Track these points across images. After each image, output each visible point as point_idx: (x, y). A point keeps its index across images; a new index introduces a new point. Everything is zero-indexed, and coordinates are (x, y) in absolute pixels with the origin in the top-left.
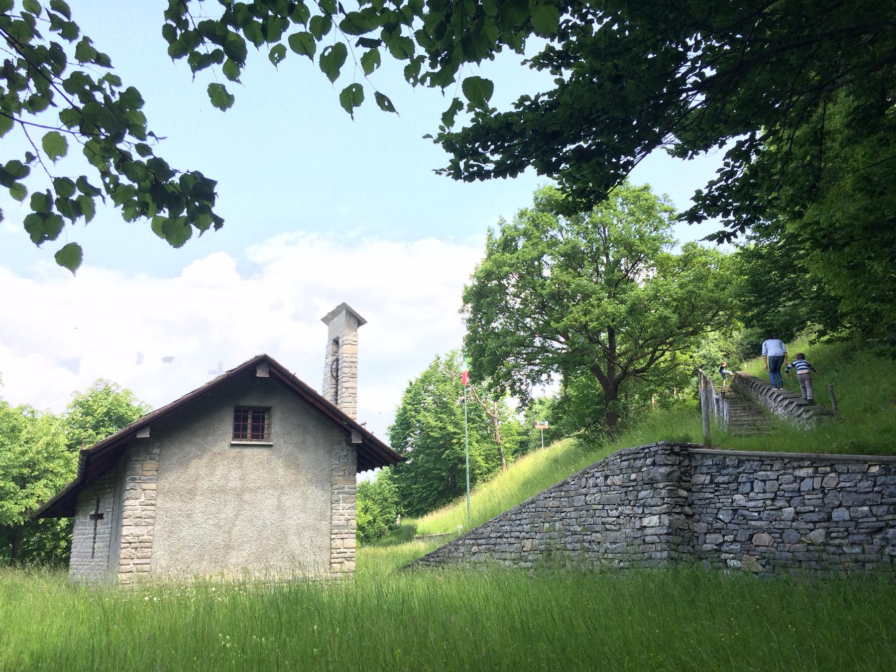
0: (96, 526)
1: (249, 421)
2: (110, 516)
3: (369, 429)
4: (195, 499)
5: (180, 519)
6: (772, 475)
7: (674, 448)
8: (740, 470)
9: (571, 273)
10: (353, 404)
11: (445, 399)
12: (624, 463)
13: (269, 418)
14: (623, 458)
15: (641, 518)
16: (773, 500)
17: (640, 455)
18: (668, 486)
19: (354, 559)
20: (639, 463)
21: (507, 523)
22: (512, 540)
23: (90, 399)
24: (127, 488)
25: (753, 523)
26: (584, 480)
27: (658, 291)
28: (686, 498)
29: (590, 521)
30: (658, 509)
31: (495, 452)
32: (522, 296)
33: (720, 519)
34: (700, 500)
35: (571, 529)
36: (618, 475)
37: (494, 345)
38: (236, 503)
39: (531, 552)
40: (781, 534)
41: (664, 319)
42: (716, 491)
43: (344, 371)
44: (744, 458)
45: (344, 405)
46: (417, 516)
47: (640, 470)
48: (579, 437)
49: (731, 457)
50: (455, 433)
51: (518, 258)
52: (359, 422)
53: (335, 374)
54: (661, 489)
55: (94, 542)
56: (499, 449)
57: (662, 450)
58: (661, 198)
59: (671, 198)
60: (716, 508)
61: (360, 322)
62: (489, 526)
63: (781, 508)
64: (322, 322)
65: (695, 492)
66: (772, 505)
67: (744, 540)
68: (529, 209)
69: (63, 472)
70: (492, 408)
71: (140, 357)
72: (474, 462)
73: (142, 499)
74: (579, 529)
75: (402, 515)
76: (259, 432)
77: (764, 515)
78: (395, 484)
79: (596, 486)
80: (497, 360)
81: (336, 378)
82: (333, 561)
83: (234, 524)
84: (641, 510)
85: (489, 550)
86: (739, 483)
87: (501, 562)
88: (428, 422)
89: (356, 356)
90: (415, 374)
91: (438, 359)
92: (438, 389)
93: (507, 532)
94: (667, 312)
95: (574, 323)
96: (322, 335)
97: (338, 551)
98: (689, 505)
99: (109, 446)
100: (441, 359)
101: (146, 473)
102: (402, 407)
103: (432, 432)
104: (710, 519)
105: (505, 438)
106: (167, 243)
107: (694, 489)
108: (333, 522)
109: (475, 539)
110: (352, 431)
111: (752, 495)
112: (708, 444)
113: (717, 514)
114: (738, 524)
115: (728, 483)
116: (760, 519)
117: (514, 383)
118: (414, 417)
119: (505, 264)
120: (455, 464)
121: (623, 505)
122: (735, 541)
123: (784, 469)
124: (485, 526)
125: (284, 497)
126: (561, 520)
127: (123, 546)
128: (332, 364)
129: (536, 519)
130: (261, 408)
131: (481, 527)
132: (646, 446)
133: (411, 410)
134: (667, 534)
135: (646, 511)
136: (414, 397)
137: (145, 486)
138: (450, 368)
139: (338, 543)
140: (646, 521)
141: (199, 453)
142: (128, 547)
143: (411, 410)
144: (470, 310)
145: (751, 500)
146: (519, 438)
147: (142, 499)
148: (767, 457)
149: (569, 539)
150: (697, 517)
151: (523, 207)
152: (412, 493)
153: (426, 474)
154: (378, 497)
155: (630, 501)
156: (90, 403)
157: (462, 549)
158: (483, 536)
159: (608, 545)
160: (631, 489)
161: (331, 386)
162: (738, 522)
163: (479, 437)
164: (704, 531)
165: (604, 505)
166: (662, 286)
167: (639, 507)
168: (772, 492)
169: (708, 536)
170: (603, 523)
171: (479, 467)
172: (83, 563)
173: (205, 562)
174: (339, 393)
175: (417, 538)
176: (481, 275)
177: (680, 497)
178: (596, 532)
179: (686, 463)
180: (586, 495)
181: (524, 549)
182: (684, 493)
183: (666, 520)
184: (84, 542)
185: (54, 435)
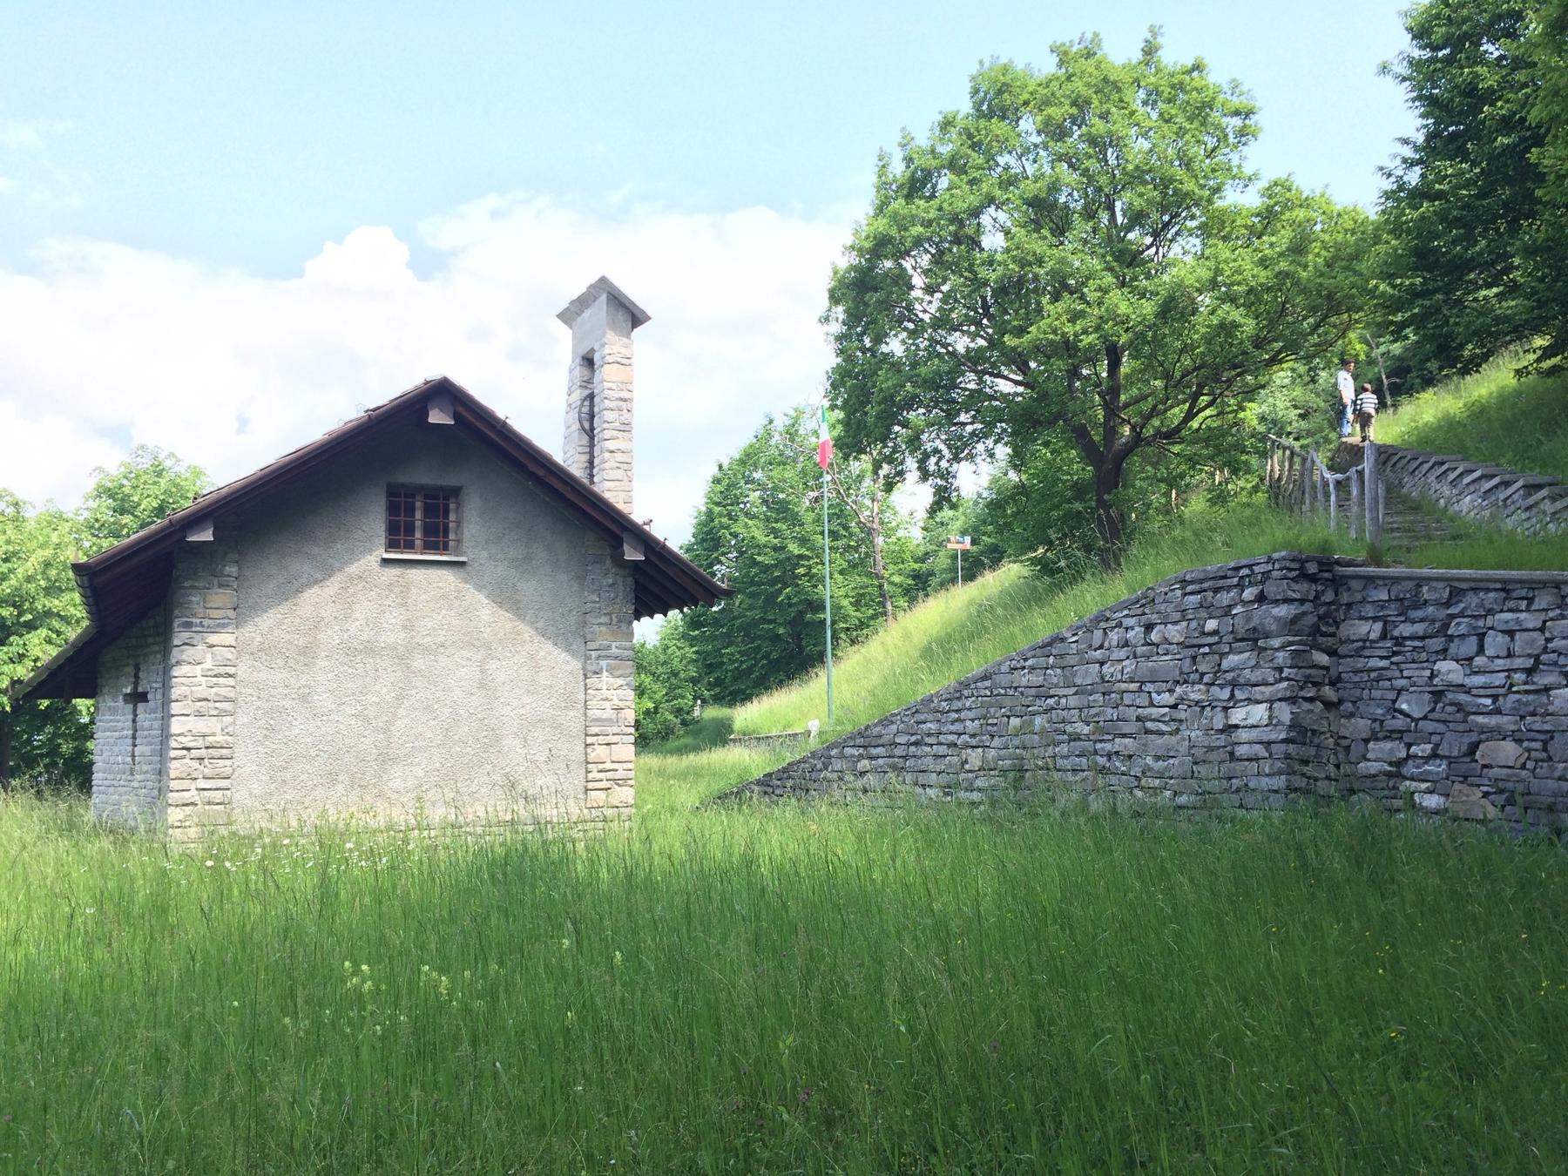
0: (135, 710)
1: (418, 515)
2: (159, 697)
3: (658, 531)
4: (314, 664)
5: (288, 704)
6: (1531, 620)
7: (1307, 565)
8: (1453, 610)
9: (1045, 238)
10: (626, 482)
11: (781, 496)
12: (1191, 598)
13: (457, 511)
14: (1189, 588)
15: (1226, 709)
16: (1529, 672)
17: (1228, 582)
18: (1291, 643)
19: (632, 782)
20: (1225, 598)
21: (931, 717)
22: (942, 750)
23: (125, 482)
24: (176, 642)
25: (1480, 719)
26: (1098, 634)
27: (1218, 272)
28: (1327, 668)
29: (1111, 713)
30: (1267, 690)
31: (876, 591)
32: (945, 288)
33: (1402, 712)
34: (1356, 672)
35: (1069, 729)
36: (1175, 623)
37: (890, 383)
38: (398, 674)
39: (982, 773)
40: (1545, 743)
41: (1228, 328)
42: (1395, 654)
43: (608, 417)
44: (1464, 586)
45: (608, 485)
46: (732, 704)
47: (1227, 611)
48: (1034, 561)
49: (1434, 584)
50: (801, 557)
51: (940, 209)
52: (638, 517)
53: (587, 426)
54: (1277, 650)
55: (135, 745)
56: (881, 586)
57: (1281, 569)
58: (1226, 87)
59: (1244, 88)
60: (1392, 689)
61: (635, 318)
62: (892, 723)
63: (1547, 689)
64: (649, 314)
65: (1345, 657)
66: (1526, 683)
67: (1455, 753)
68: (961, 116)
69: (79, 615)
70: (868, 513)
71: (243, 424)
72: (837, 608)
73: (208, 664)
74: (1086, 730)
75: (704, 701)
76: (438, 537)
77: (1508, 702)
78: (692, 646)
79: (1126, 644)
80: (892, 412)
81: (590, 433)
82: (590, 785)
83: (395, 714)
84: (1226, 694)
85: (894, 767)
86: (1451, 638)
87: (919, 790)
88: (753, 537)
89: (629, 387)
90: (730, 450)
91: (771, 422)
92: (769, 478)
93: (929, 735)
94: (1236, 315)
95: (1051, 336)
96: (563, 344)
97: (601, 766)
98: (1332, 684)
99: (135, 553)
100: (775, 423)
101: (213, 613)
102: (704, 509)
103: (759, 554)
104: (1380, 711)
105: (891, 566)
106: (380, 403)
107: (1342, 650)
108: (590, 713)
109: (865, 747)
110: (625, 536)
111: (1479, 661)
112: (1375, 558)
113: (1394, 701)
114: (1445, 722)
115: (1422, 638)
116: (1498, 712)
117: (926, 456)
118: (727, 528)
119: (913, 220)
120: (801, 614)
121: (1186, 682)
122: (1434, 755)
123: (1559, 607)
124: (886, 721)
125: (492, 665)
126: (1046, 712)
127: (173, 754)
128: (582, 405)
129: (992, 710)
130: (441, 488)
131: (876, 725)
132: (1244, 562)
133: (721, 515)
134: (1284, 741)
135: (1239, 695)
136: (726, 492)
137: (213, 639)
138: (792, 440)
139: (599, 752)
140: (1237, 716)
141: (318, 576)
142: (183, 757)
143: (721, 515)
144: (842, 316)
145: (1476, 673)
146: (916, 566)
147: (208, 664)
148: (1521, 581)
149: (1064, 749)
150: (1348, 707)
151: (949, 108)
152: (723, 663)
153: (748, 629)
154: (661, 670)
155: (1203, 674)
156: (127, 490)
157: (837, 764)
158: (880, 742)
159: (1149, 761)
160: (1207, 650)
161: (580, 449)
162: (1444, 716)
163: (845, 565)
164: (1364, 736)
165: (1143, 683)
166: (1226, 261)
167: (1222, 686)
168: (1529, 656)
169: (1371, 745)
170: (1139, 719)
171: (845, 618)
172: (115, 783)
173: (340, 787)
174: (596, 461)
175: (734, 740)
176: (867, 245)
177: (1315, 666)
178: (1124, 736)
179: (1329, 596)
180: (1102, 664)
181: (967, 767)
182: (1323, 659)
183: (1285, 713)
184: (115, 744)
185: (58, 547)
